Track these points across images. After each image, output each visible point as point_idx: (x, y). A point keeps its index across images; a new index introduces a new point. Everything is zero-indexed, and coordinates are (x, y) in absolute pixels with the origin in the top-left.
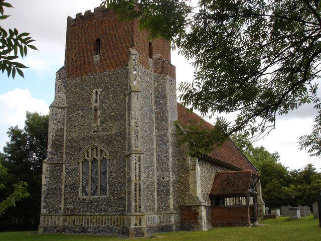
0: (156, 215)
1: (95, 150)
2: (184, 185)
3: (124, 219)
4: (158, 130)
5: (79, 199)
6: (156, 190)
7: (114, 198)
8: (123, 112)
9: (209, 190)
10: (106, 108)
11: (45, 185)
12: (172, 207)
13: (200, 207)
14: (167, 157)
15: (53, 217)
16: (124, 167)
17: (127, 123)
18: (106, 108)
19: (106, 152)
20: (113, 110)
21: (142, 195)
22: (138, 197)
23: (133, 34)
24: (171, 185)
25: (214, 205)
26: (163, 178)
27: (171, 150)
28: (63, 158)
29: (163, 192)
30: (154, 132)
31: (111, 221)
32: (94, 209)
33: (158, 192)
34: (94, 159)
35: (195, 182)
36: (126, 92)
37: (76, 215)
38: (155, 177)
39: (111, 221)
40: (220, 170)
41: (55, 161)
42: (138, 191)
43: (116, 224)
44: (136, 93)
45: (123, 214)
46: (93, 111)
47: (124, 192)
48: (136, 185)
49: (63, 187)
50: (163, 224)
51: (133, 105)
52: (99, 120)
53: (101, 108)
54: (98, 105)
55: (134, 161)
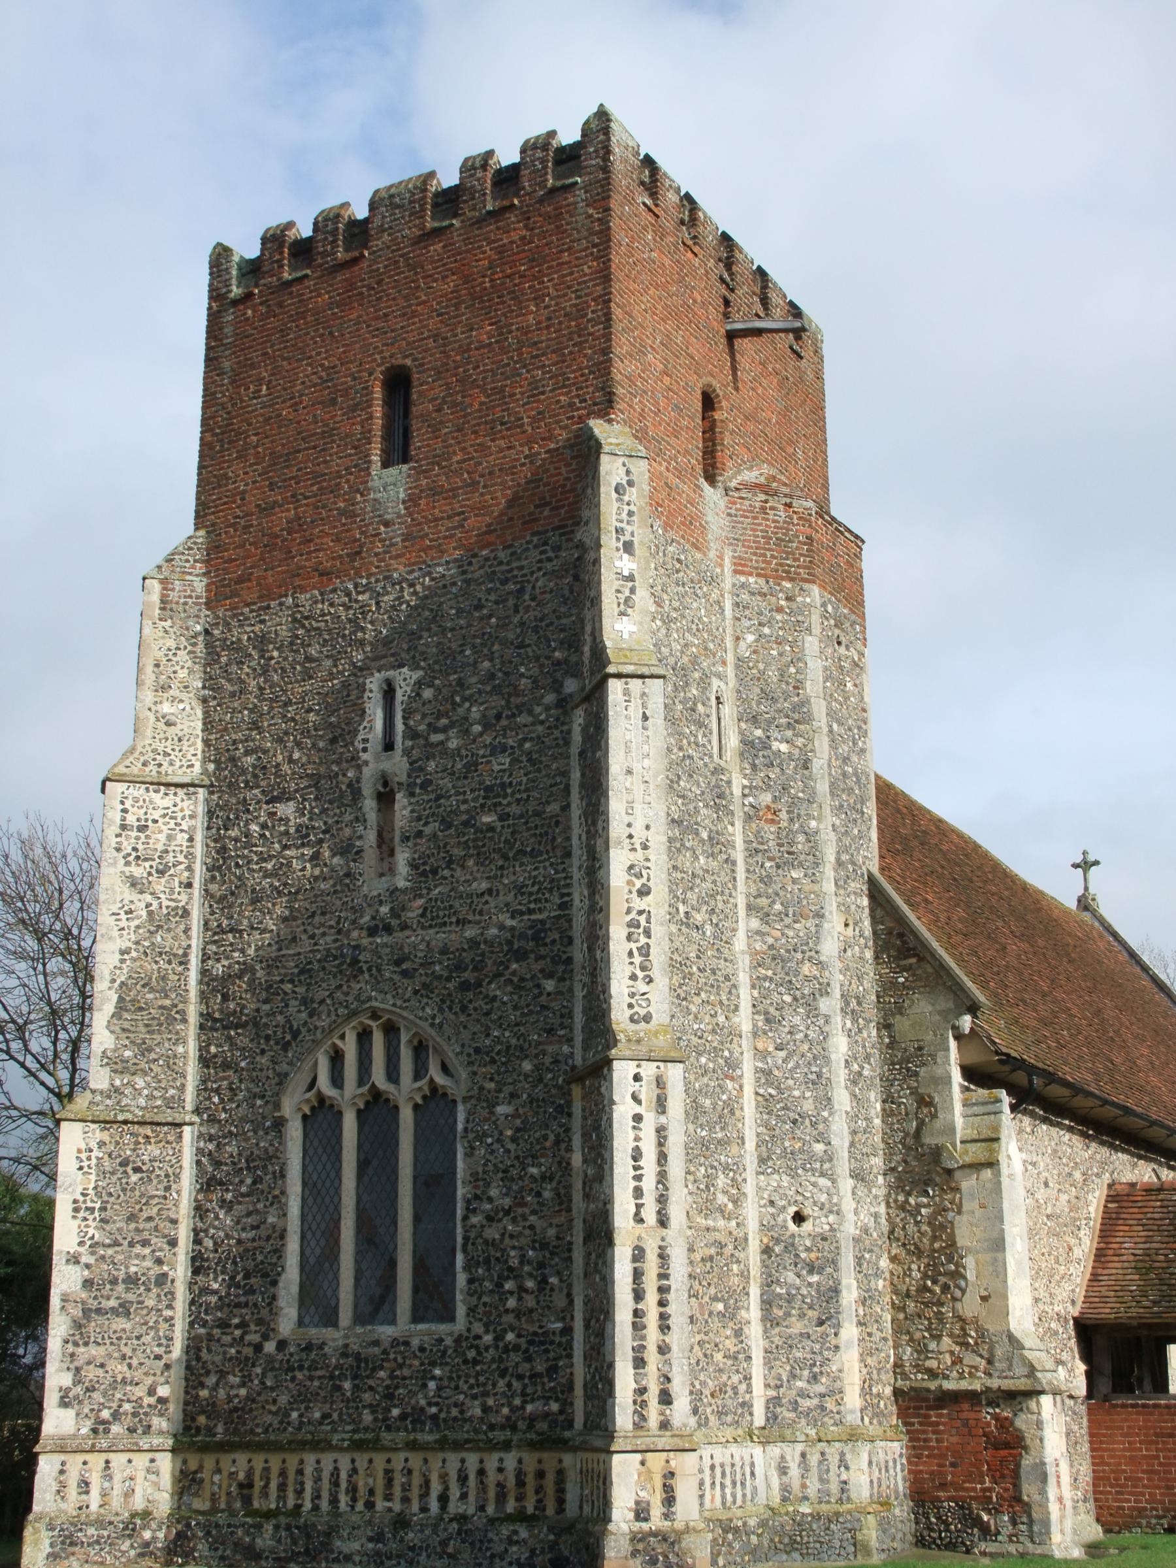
0: (758, 1451)
1: (378, 1039)
2: (934, 1274)
3: (561, 1473)
4: (765, 918)
5: (282, 1345)
6: (755, 1291)
7: (499, 1337)
8: (553, 808)
9: (1070, 1292)
10: (446, 783)
11: (74, 1259)
12: (853, 1399)
13: (1033, 1404)
14: (819, 1082)
15: (118, 1460)
16: (563, 1140)
17: (577, 874)
18: (446, 783)
19: (451, 1052)
20: (492, 794)
21: (678, 1320)
22: (653, 1334)
23: (608, 337)
24: (847, 1260)
25: (1104, 1386)
26: (799, 1218)
27: (840, 1046)
28: (182, 1088)
29: (800, 1286)
30: (741, 935)
31: (482, 1487)
32: (373, 1408)
33: (767, 1304)
34: (376, 1095)
35: (998, 1244)
36: (571, 686)
37: (261, 1447)
38: (752, 1213)
39: (482, 1487)
40: (1142, 1172)
41: (136, 1106)
42: (652, 1297)
43: (511, 1506)
44: (635, 684)
45: (562, 1444)
46: (369, 805)
47: (560, 1301)
48: (639, 1255)
49: (180, 1271)
50: (805, 1509)
51: (616, 762)
52: (402, 858)
53: (418, 782)
54: (398, 765)
55: (632, 1108)
